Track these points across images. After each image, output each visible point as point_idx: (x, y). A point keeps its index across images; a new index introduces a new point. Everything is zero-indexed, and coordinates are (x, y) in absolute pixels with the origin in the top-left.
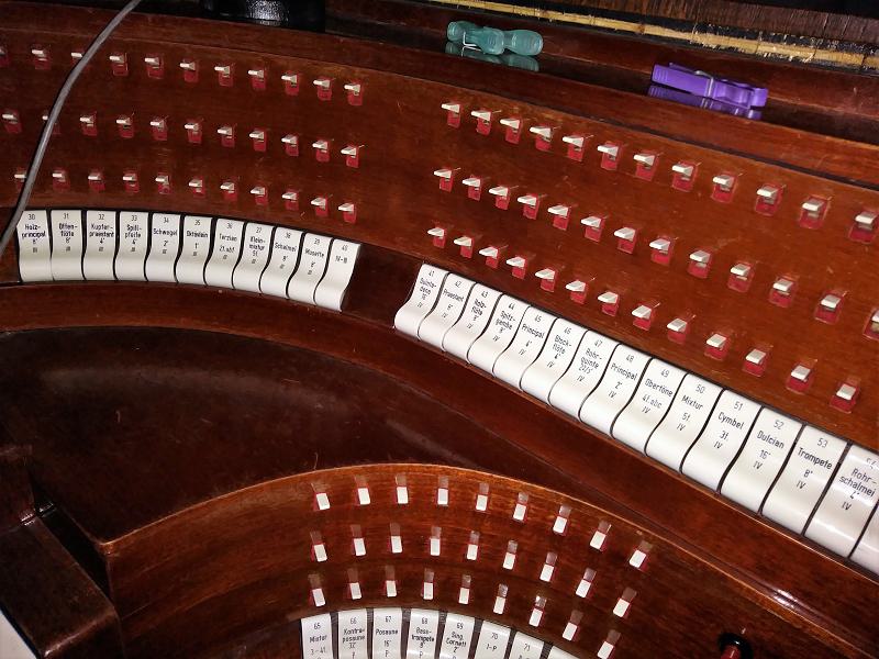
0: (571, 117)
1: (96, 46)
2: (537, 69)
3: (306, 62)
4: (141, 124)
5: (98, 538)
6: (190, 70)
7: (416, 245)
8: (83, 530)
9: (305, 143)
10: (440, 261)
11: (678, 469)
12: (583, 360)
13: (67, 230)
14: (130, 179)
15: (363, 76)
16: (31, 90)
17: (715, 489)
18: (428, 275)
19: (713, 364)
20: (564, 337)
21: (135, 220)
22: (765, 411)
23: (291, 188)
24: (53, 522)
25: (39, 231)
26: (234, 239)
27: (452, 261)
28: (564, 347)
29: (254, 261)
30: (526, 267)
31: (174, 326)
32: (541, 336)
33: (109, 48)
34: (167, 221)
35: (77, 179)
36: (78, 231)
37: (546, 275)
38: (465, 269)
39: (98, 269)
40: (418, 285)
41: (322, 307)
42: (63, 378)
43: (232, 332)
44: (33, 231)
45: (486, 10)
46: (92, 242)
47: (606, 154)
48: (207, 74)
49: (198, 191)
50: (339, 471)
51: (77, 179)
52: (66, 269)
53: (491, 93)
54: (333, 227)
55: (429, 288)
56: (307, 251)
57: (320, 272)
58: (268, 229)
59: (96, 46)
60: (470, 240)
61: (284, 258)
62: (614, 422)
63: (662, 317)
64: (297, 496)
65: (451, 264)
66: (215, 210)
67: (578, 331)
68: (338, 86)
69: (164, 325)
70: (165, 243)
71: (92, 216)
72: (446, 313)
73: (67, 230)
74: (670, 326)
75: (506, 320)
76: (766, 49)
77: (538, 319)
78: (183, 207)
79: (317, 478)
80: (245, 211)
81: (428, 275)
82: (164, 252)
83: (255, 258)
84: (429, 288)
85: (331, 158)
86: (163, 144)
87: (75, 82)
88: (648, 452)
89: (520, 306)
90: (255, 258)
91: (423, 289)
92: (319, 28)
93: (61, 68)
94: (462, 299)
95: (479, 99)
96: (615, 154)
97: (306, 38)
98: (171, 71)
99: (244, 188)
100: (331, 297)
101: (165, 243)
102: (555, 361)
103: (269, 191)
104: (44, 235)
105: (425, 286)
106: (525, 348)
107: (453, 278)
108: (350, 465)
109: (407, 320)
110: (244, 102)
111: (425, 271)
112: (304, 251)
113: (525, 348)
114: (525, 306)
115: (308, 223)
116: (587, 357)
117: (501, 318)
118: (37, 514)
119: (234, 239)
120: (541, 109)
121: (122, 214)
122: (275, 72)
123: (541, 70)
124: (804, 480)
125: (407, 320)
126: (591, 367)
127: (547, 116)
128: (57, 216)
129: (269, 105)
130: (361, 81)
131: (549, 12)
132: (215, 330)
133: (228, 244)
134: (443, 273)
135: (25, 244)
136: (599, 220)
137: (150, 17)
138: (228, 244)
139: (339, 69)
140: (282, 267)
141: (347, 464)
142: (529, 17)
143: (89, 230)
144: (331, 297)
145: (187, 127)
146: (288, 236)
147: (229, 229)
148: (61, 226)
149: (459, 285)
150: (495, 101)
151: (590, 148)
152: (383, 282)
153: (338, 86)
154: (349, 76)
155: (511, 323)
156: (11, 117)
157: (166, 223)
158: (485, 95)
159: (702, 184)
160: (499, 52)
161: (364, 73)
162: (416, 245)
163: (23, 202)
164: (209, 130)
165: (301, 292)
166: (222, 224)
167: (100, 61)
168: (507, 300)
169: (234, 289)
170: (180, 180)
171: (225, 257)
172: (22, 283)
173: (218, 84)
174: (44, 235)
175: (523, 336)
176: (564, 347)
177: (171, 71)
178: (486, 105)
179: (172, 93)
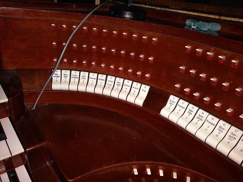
0: (235, 53)
1: (80, 24)
2: (218, 35)
3: (141, 31)
4: (90, 47)
5: (68, 178)
6: (105, 32)
7: (169, 88)
8: (60, 169)
9: (137, 55)
10: (177, 95)
11: (204, 142)
12: (230, 136)
13: (65, 76)
14: (85, 63)
15: (158, 36)
16: (62, 36)
17: (227, 156)
18: (173, 99)
19: (187, 96)
20: (223, 127)
21: (85, 74)
22: (190, 104)
23: (131, 68)
24: (54, 166)
25: (58, 76)
26: (112, 82)
27: (181, 95)
28: (222, 130)
29: (117, 89)
30: (210, 101)
31: (92, 106)
32: (214, 125)
33: (83, 25)
34: (93, 75)
35: (70, 62)
36: (69, 77)
37: (196, 94)
38: (186, 98)
39: (73, 88)
40: (169, 101)
41: (136, 105)
42: (60, 117)
43: (109, 109)
44: (57, 76)
45: (198, 16)
46: (72, 79)
47: (198, 51)
48: (110, 33)
49: (103, 67)
50: (142, 163)
51: (70, 62)
52: (64, 87)
53: (204, 43)
54: (142, 80)
55: (173, 103)
56: (133, 87)
57: (136, 93)
58: (122, 80)
59: (80, 24)
60: (189, 89)
61: (126, 89)
62: (217, 145)
63: (213, 102)
64: (127, 168)
65: (181, 96)
66: (107, 72)
67: (228, 126)
68: (150, 38)
69: (90, 105)
70: (92, 81)
71: (73, 72)
72: (178, 112)
73: (65, 76)
74: (227, 111)
75: (200, 118)
76: (185, 12)
77: (213, 119)
78: (99, 72)
79: (134, 164)
80: (116, 74)
81: (173, 99)
82: (92, 84)
83: (118, 88)
84: (173, 103)
85: (144, 60)
86: (95, 53)
87: (74, 35)
88: (217, 149)
89: (206, 114)
90: (118, 88)
91: (170, 103)
92: (143, 20)
93: (70, 30)
94: (214, 125)
95: (199, 45)
96: (201, 52)
97: (142, 23)
98: (100, 31)
99: (116, 67)
100: (140, 102)
101: (92, 81)
102: (219, 135)
103: (124, 68)
104: (59, 77)
105: (171, 102)
106: (207, 128)
107: (181, 101)
108: (146, 161)
109: (164, 112)
110: (120, 42)
111: (172, 97)
112: (132, 87)
113: (207, 128)
114: (208, 114)
115: (134, 78)
116: (232, 135)
117: (199, 117)
118: (50, 162)
119: (112, 82)
120: (223, 50)
121: (81, 72)
122: (130, 34)
123: (219, 36)
124: (179, 112)
125: (164, 112)
126: (233, 139)
127: (224, 52)
128: (63, 71)
129: (128, 43)
130: (157, 37)
131: (222, 17)
132: (104, 108)
133: (110, 83)
134: (178, 99)
135: (54, 79)
136: (228, 84)
137: (96, 16)
138: (110, 83)
139: (151, 33)
140: (125, 91)
141: (144, 161)
142: (214, 18)
143: (72, 76)
144: (140, 102)
145: (103, 48)
146: (128, 82)
147: (111, 78)
148: (64, 74)
149: (183, 103)
150: (205, 46)
151: (205, 52)
152: (157, 99)
153: (150, 38)
154: (154, 36)
155: (236, 137)
156: (55, 44)
157: (93, 75)
158: (201, 44)
159: (215, 58)
160: (206, 30)
161: (159, 35)
162: (169, 88)
163: (56, 68)
164: (108, 49)
165: (131, 99)
166: (109, 77)
167: (81, 28)
168: (201, 111)
169: (111, 97)
170: (98, 64)
171: (109, 87)
172: (52, 90)
173: (113, 37)
174: (59, 77)
175: (206, 124)
176: (222, 130)
177: (100, 31)
178: (201, 47)
179: (99, 38)
